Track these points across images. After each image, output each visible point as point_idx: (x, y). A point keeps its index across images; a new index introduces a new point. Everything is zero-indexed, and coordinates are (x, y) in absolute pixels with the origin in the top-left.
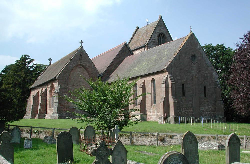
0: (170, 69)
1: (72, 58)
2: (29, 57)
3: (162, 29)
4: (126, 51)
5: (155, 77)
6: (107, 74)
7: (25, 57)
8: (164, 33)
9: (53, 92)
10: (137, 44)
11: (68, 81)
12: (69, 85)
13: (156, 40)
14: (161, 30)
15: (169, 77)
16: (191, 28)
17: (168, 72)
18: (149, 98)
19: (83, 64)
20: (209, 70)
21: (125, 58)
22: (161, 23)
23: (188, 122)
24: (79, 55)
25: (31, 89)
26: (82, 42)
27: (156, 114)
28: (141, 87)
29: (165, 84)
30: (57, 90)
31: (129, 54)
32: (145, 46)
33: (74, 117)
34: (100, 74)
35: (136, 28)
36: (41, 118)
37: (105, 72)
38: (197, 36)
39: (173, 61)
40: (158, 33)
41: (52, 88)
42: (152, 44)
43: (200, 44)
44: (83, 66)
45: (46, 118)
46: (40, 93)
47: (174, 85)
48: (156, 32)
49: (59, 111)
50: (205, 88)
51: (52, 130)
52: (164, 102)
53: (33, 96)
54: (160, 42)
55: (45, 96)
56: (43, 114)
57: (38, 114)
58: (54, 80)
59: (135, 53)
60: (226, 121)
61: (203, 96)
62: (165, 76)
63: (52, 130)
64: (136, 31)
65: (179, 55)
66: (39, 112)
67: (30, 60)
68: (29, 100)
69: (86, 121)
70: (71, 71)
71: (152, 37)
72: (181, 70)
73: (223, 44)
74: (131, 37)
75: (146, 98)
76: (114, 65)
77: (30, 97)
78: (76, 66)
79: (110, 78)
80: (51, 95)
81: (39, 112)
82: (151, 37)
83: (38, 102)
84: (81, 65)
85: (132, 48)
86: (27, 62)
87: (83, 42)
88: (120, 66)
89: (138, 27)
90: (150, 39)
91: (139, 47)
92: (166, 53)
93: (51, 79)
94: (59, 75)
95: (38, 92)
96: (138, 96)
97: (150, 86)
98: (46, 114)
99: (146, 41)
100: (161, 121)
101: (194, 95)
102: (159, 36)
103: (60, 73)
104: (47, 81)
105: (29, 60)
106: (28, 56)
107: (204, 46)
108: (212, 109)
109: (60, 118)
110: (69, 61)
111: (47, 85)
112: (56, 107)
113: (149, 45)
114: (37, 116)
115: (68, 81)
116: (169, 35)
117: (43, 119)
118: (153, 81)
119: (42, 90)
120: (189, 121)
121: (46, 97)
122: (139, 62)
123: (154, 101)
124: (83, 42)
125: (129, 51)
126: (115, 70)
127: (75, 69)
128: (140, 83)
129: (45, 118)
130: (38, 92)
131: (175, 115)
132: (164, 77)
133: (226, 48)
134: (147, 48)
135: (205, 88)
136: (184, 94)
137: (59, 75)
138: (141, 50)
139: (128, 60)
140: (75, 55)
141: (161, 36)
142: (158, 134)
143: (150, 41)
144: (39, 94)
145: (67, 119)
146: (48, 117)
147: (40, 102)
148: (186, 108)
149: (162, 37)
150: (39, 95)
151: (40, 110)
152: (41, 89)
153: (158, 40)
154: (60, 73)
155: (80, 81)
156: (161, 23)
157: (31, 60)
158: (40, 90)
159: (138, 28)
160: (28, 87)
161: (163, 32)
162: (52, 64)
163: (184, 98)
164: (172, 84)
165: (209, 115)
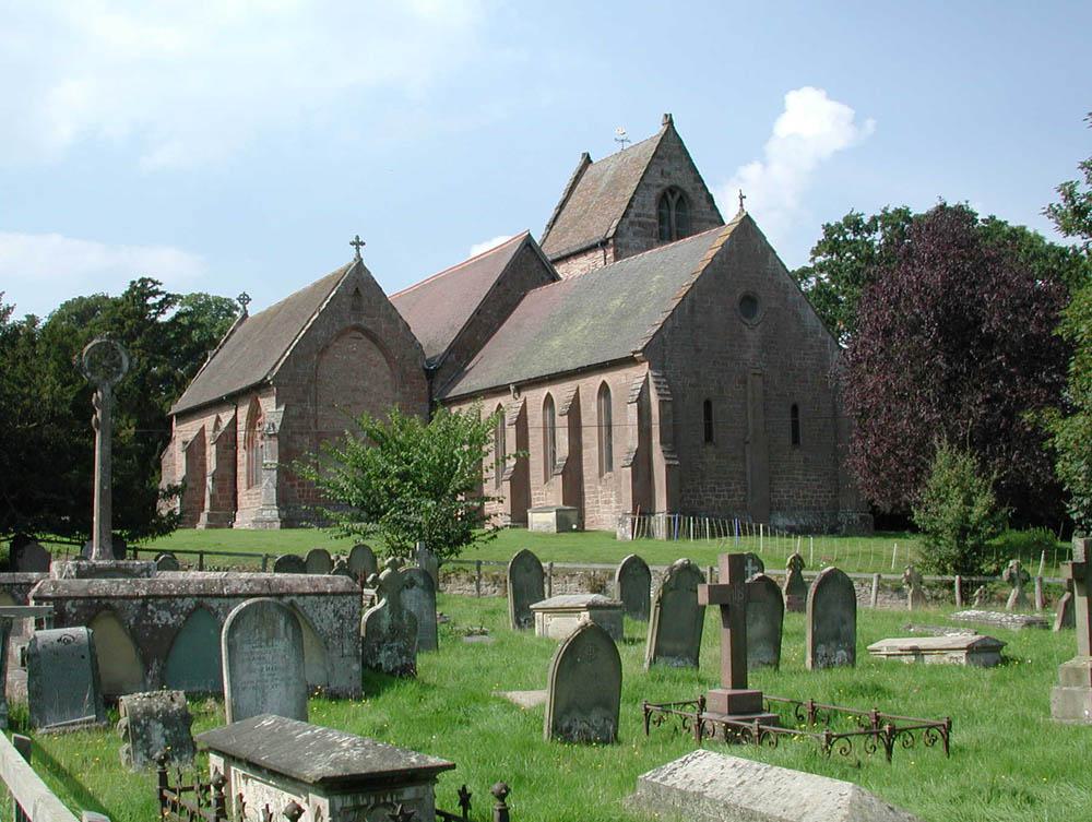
0: (656, 352)
1: (322, 303)
2: (161, 284)
3: (676, 169)
4: (530, 266)
5: (609, 377)
6: (458, 358)
7: (144, 286)
8: (682, 187)
9: (257, 429)
10: (580, 232)
11: (312, 388)
12: (316, 403)
13: (650, 217)
14: (669, 174)
15: (651, 380)
16: (742, 197)
17: (647, 364)
18: (591, 453)
19: (365, 322)
20: (812, 347)
21: (524, 296)
22: (670, 148)
23: (699, 534)
24: (351, 291)
25: (172, 415)
26: (358, 244)
27: (613, 505)
28: (566, 410)
29: (636, 404)
30: (273, 425)
31: (542, 278)
32: (604, 244)
33: (324, 523)
34: (427, 357)
35: (578, 162)
36: (217, 527)
37: (451, 349)
38: (762, 225)
39: (669, 325)
40: (659, 186)
41: (254, 415)
42: (634, 234)
43: (774, 252)
44: (367, 333)
45: (235, 526)
46: (208, 434)
47: (669, 407)
48: (648, 186)
49: (283, 501)
50: (795, 409)
51: (261, 559)
52: (635, 465)
53: (185, 443)
54: (667, 220)
55: (228, 442)
56: (225, 512)
57: (207, 511)
58: (260, 388)
59: (560, 270)
60: (872, 528)
61: (787, 438)
62: (638, 375)
63: (261, 559)
64: (580, 171)
65: (693, 300)
66: (207, 505)
67: (164, 296)
68: (166, 459)
69: (354, 532)
70: (322, 352)
71: (634, 204)
72: (698, 351)
73: (964, 204)
74: (561, 197)
75: (584, 451)
76: (484, 321)
77: (170, 446)
78: (341, 334)
79: (468, 371)
80: (250, 441)
81: (207, 505)
82: (630, 206)
83: (203, 465)
84: (357, 328)
85: (550, 252)
86: (154, 306)
87: (363, 244)
88: (505, 325)
89: (588, 157)
90: (625, 215)
91: (584, 246)
92: (653, 289)
93: (249, 384)
94: (277, 368)
95: (203, 430)
96: (507, 455)
97: (594, 408)
98: (236, 510)
99: (605, 222)
100: (625, 532)
101: (748, 438)
102: (663, 200)
103: (282, 361)
104: (240, 387)
105: (160, 298)
106: (153, 282)
107: (879, 213)
108: (819, 486)
109: (288, 522)
110: (315, 317)
111: (234, 404)
112: (271, 484)
113: (619, 240)
114: (204, 517)
115: (312, 388)
116: (705, 193)
117: (226, 531)
118: (604, 390)
119: (218, 419)
120: (719, 530)
121: (230, 452)
122: (569, 315)
123: (607, 463)
124: (363, 244)
125: (540, 265)
126: (487, 341)
127: (336, 344)
128: (564, 397)
129: (232, 526)
130: (203, 430)
131: (671, 510)
132: (637, 381)
133: (979, 217)
134: (612, 250)
135: (795, 409)
136: (709, 438)
137: (277, 368)
138: (590, 255)
139: (536, 302)
140: (334, 292)
141: (670, 197)
142: (551, 565)
143: (626, 221)
144: (207, 434)
145: (302, 527)
146: (243, 520)
147: (211, 465)
148: (715, 483)
149: (673, 201)
150: (207, 441)
151: (211, 496)
152: (215, 416)
153: (660, 215)
154: (282, 361)
155: (355, 390)
156: (670, 148)
157: (168, 296)
158: (208, 421)
159: (588, 161)
160: (162, 406)
161: (679, 183)
162: (250, 315)
163: (710, 448)
164: (662, 403)
165: (807, 508)
